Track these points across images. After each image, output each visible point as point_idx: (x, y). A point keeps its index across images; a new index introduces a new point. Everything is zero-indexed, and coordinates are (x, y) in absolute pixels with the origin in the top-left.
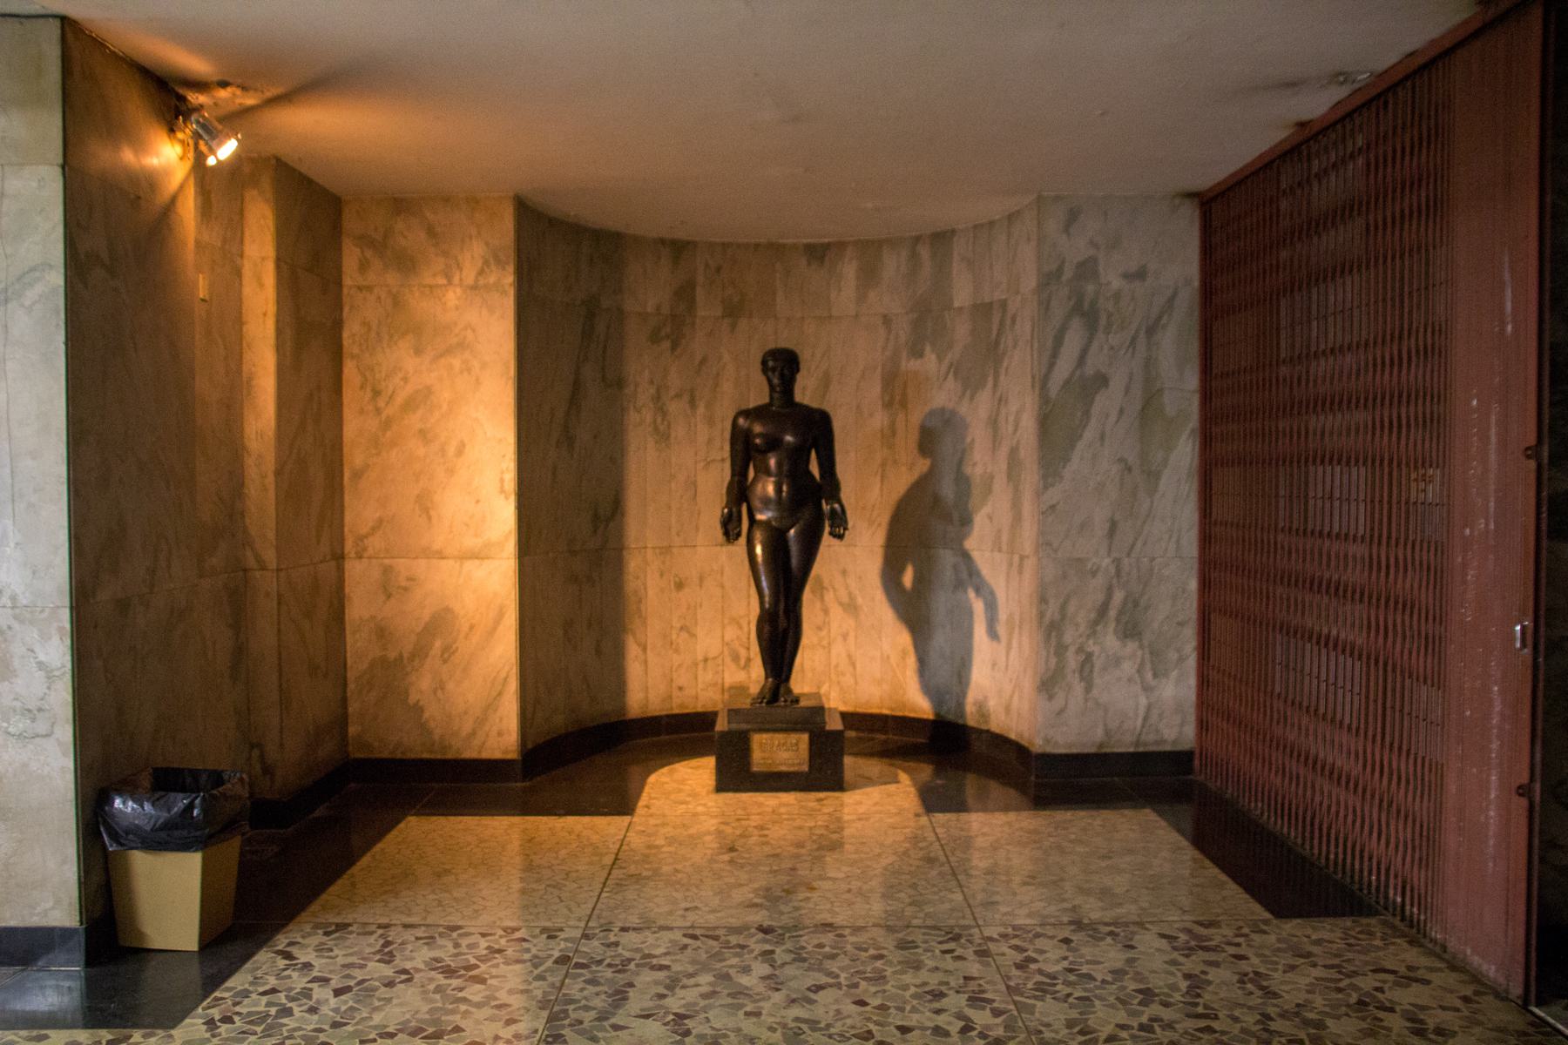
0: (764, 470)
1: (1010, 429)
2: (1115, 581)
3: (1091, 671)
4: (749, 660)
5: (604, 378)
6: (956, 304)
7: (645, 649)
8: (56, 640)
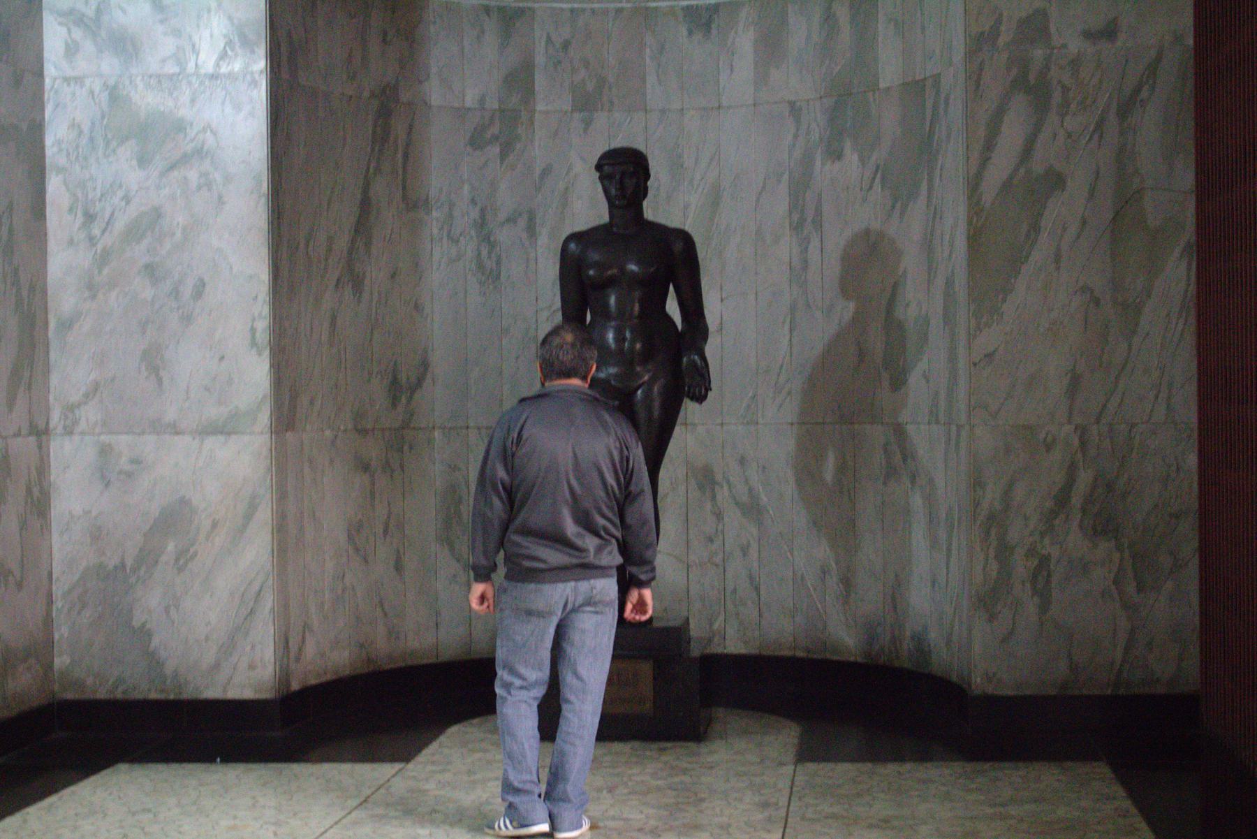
1: (946, 253)
2: (1079, 455)
3: (1048, 582)
5: (405, 197)
6: (882, 85)
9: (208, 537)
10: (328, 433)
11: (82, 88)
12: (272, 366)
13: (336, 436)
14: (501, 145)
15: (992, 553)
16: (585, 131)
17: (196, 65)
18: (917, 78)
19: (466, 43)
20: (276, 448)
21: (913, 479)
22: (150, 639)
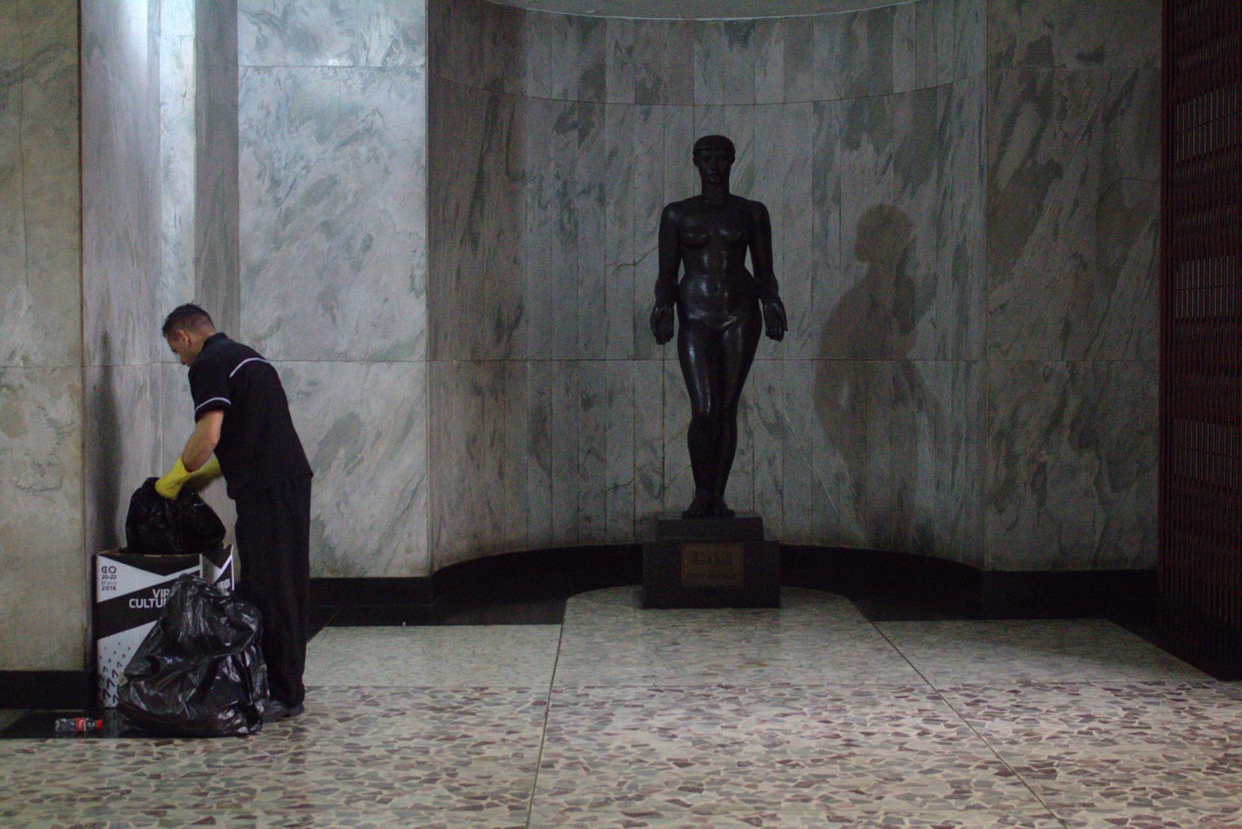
0: (695, 268)
5: (508, 173)
6: (896, 90)
8: (65, 398)
9: (373, 446)
10: (455, 362)
11: (270, 76)
12: (428, 306)
15: (1001, 462)
16: (645, 120)
17: (367, 59)
18: (928, 87)
21: (920, 406)
22: (323, 530)
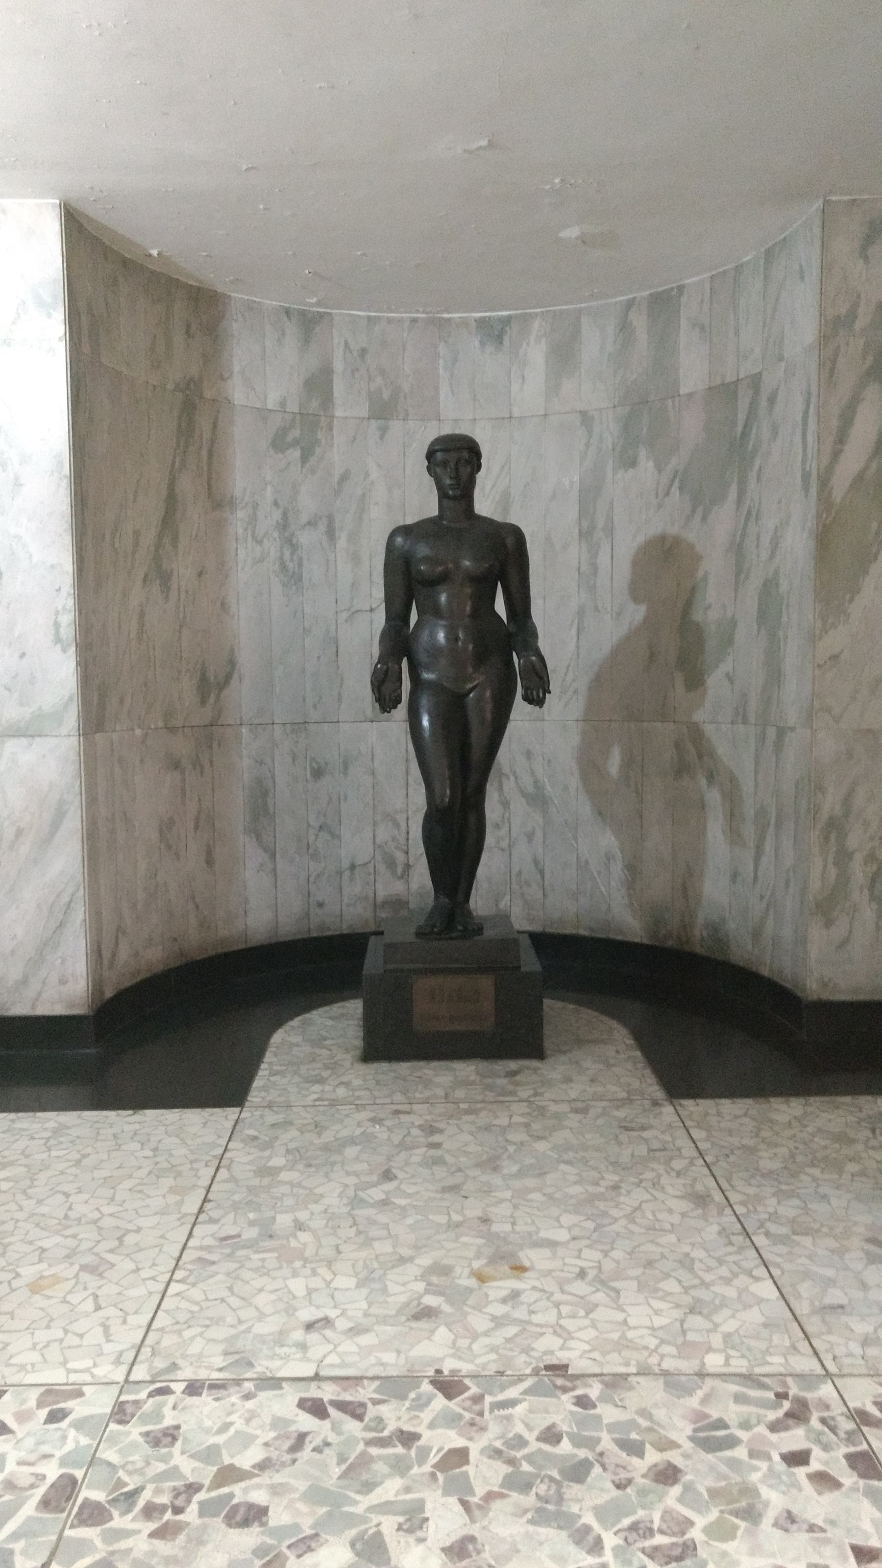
0: (430, 611)
1: (764, 555)
4: (408, 867)
5: (210, 494)
7: (273, 855)
10: (138, 732)
13: (146, 735)
14: (302, 449)
15: (831, 859)
16: (382, 437)
18: (728, 379)
19: (268, 344)
20: (84, 750)
